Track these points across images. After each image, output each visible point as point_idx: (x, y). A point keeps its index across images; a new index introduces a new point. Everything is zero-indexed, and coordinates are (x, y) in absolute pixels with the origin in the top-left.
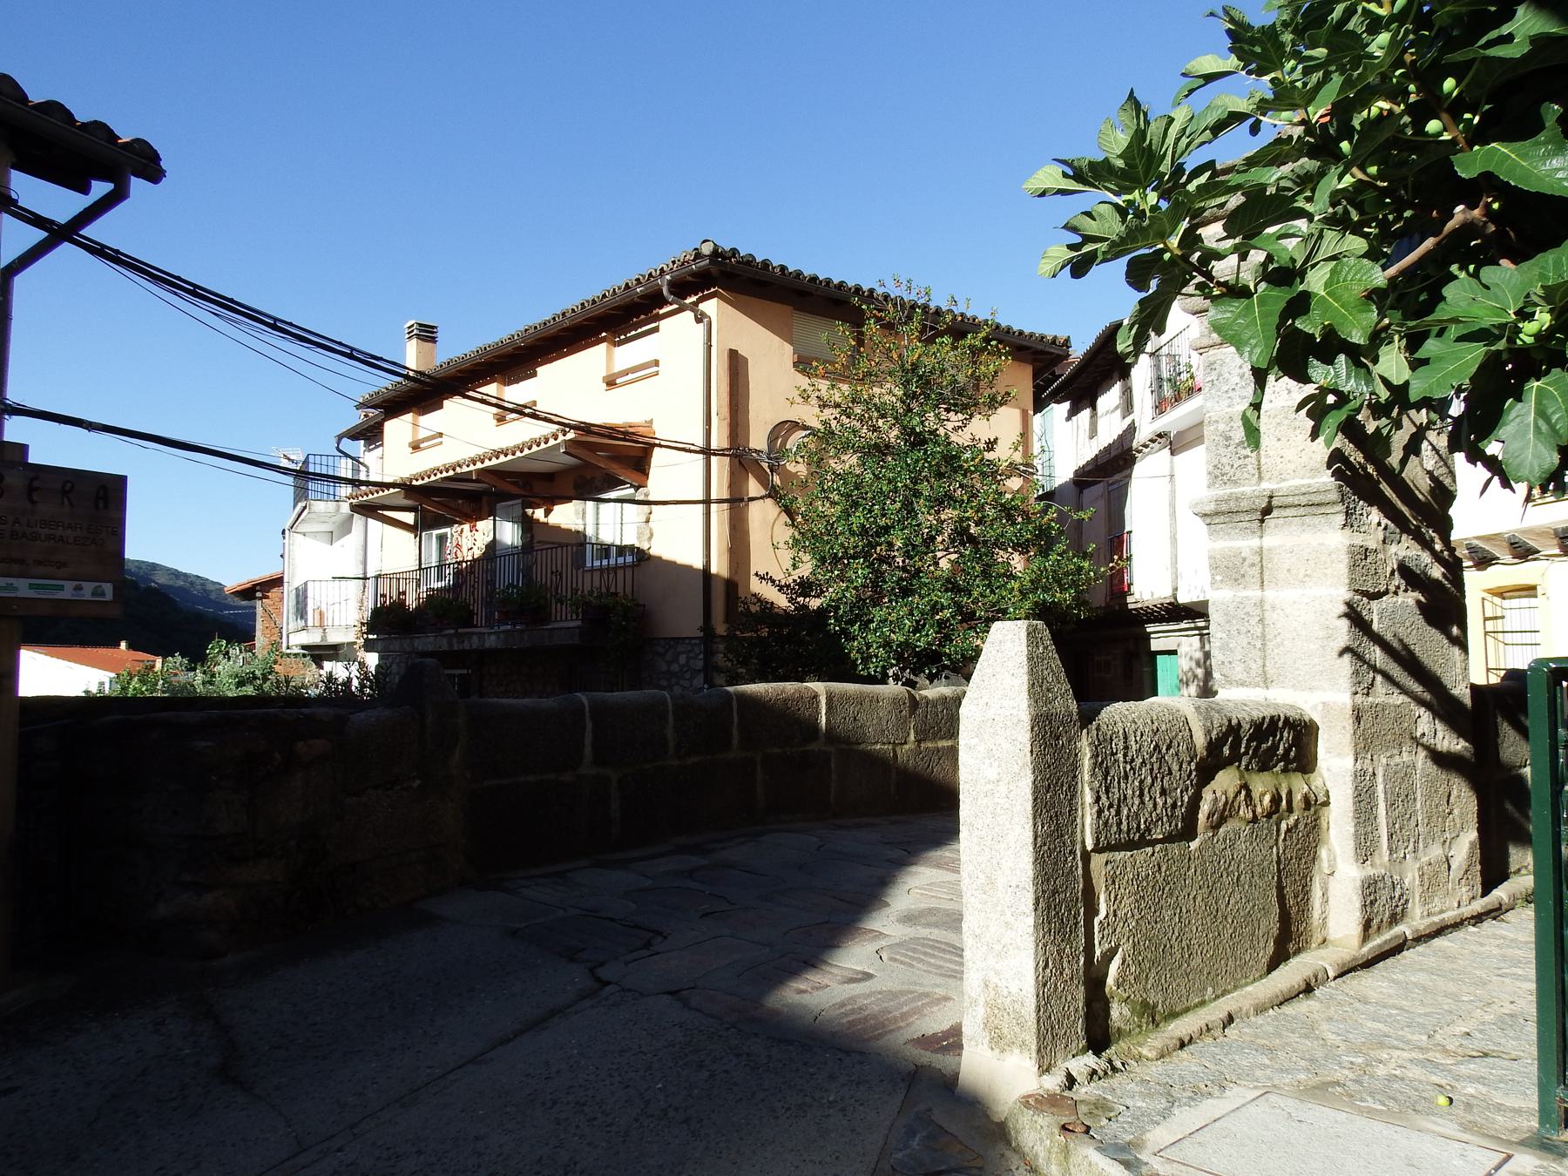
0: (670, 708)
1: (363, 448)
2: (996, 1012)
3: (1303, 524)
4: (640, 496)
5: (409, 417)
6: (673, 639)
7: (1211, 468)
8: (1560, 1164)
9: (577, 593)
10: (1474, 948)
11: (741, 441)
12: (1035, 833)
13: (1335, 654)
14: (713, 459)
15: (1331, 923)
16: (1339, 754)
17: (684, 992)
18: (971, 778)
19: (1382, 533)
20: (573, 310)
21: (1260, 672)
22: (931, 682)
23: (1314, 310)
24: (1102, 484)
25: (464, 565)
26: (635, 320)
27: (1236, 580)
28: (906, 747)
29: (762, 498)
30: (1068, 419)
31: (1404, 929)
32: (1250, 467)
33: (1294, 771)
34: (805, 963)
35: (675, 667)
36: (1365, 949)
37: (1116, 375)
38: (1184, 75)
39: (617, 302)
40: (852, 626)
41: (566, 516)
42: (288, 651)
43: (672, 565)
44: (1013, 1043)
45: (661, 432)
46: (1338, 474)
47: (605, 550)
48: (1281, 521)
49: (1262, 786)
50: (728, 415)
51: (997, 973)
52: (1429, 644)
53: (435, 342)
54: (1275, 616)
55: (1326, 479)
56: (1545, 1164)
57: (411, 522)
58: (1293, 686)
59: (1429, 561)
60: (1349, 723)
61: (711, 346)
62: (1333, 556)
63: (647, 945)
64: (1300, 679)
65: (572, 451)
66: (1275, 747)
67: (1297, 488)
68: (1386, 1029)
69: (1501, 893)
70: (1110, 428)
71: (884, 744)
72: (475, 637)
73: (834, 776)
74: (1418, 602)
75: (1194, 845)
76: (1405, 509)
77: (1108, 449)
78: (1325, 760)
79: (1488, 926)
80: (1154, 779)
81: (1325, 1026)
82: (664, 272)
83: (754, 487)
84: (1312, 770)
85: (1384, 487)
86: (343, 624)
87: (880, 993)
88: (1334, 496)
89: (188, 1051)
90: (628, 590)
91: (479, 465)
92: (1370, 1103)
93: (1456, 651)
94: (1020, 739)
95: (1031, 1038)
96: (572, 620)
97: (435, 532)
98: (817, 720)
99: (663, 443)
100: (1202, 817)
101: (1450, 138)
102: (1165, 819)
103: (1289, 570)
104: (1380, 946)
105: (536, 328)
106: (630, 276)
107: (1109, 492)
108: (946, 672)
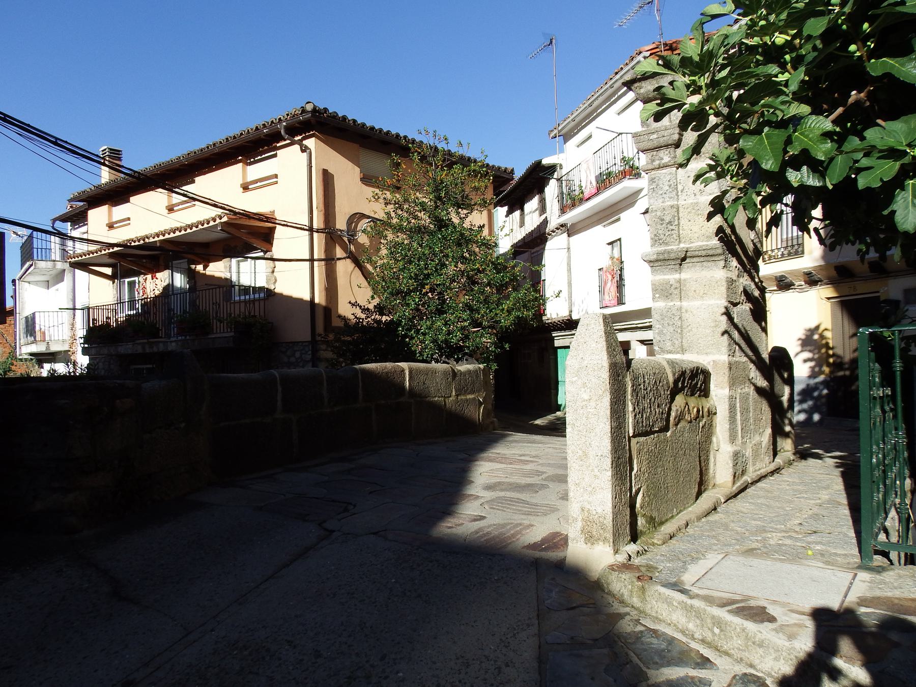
1: (70, 228)
2: (589, 523)
3: (702, 266)
4: (268, 255)
5: (105, 208)
6: (292, 342)
7: (653, 236)
8: (880, 576)
9: (231, 315)
10: (778, 486)
11: (331, 224)
12: (611, 426)
13: (719, 335)
14: (315, 235)
15: (717, 476)
16: (722, 387)
17: (381, 533)
18: (573, 399)
20: (221, 142)
21: (680, 345)
22: (457, 363)
23: (795, 142)
24: (527, 253)
25: (149, 300)
26: (261, 149)
27: (667, 297)
28: (451, 399)
29: (344, 258)
30: (507, 216)
31: (747, 478)
32: (674, 235)
33: (703, 396)
34: (443, 513)
35: (293, 359)
36: (734, 488)
37: (536, 191)
38: (702, 14)
39: (250, 138)
41: (217, 269)
42: (21, 357)
43: (289, 299)
44: (599, 539)
45: (279, 216)
46: (721, 240)
47: (246, 290)
48: (691, 264)
49: (693, 402)
50: (323, 209)
51: (589, 503)
52: (753, 329)
54: (687, 315)
55: (715, 242)
56: (873, 576)
57: (110, 273)
58: (697, 352)
60: (727, 371)
62: (719, 283)
63: (346, 510)
64: (701, 348)
66: (697, 383)
67: (701, 246)
68: (763, 524)
69: (779, 460)
70: (532, 221)
71: (439, 397)
74: (750, 308)
75: (669, 434)
76: (744, 259)
77: (531, 233)
78: (714, 391)
79: (776, 475)
80: (655, 398)
81: (732, 525)
82: (281, 120)
83: (339, 252)
84: (708, 397)
85: (737, 247)
86: (61, 338)
87: (494, 525)
88: (720, 251)
89: (87, 585)
90: (262, 314)
91: (161, 238)
92: (777, 556)
93: (764, 334)
94: (603, 376)
95: (610, 536)
96: (227, 332)
97: (127, 280)
99: (289, 224)
100: (672, 419)
101: (859, 54)
102: (659, 420)
103: (695, 291)
104: (740, 486)
105: (195, 152)
106: (259, 122)
107: (532, 258)
108: (466, 356)
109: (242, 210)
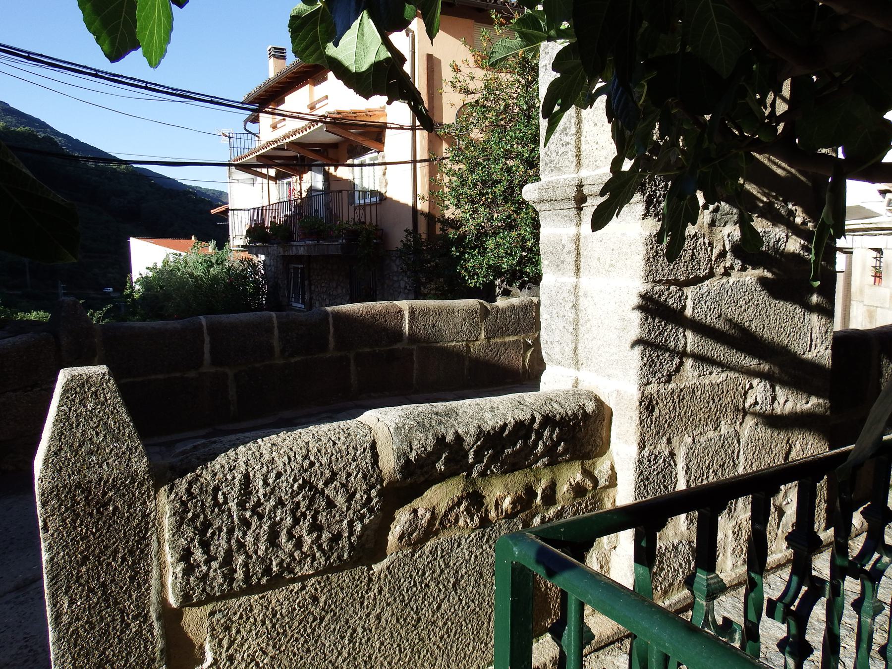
0: (276, 324)
13: (628, 345)
19: (710, 216)
28: (478, 343)
32: (570, 154)
40: (475, 250)
41: (343, 173)
43: (397, 203)
47: (365, 192)
53: (285, 59)
58: (597, 371)
59: (784, 235)
61: (414, 52)
65: (331, 130)
72: (294, 248)
73: (416, 366)
74: (762, 281)
91: (288, 140)
97: (285, 181)
98: (401, 328)
103: (599, 259)
109: (297, 113)
